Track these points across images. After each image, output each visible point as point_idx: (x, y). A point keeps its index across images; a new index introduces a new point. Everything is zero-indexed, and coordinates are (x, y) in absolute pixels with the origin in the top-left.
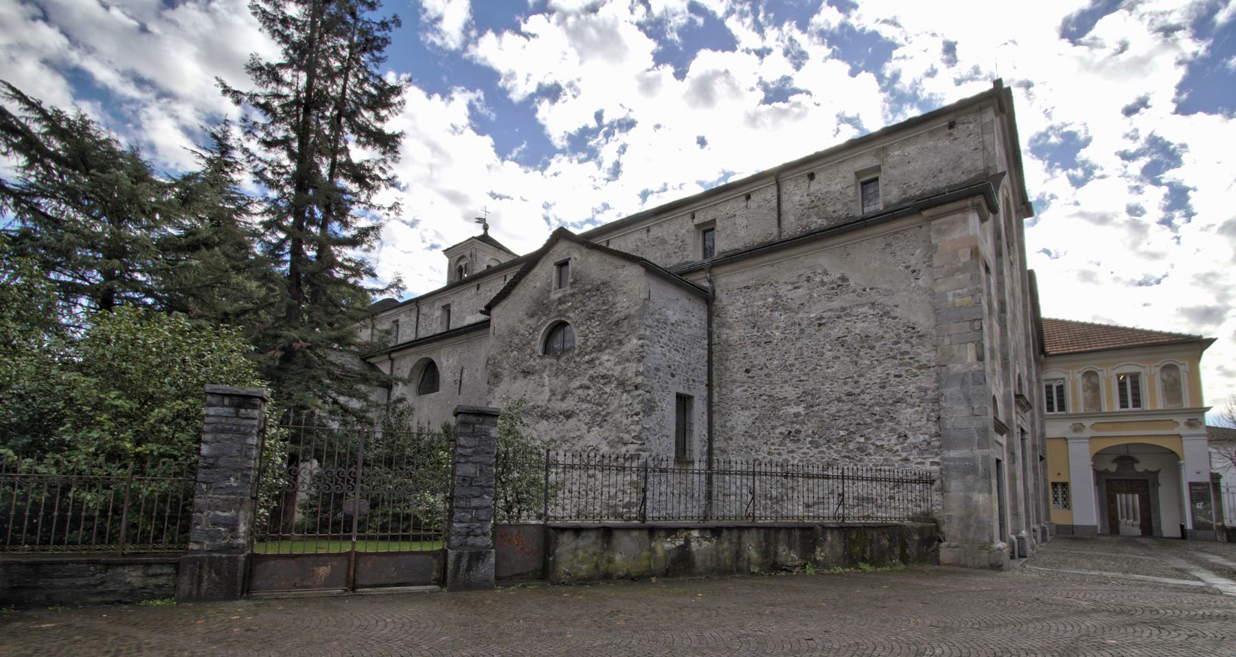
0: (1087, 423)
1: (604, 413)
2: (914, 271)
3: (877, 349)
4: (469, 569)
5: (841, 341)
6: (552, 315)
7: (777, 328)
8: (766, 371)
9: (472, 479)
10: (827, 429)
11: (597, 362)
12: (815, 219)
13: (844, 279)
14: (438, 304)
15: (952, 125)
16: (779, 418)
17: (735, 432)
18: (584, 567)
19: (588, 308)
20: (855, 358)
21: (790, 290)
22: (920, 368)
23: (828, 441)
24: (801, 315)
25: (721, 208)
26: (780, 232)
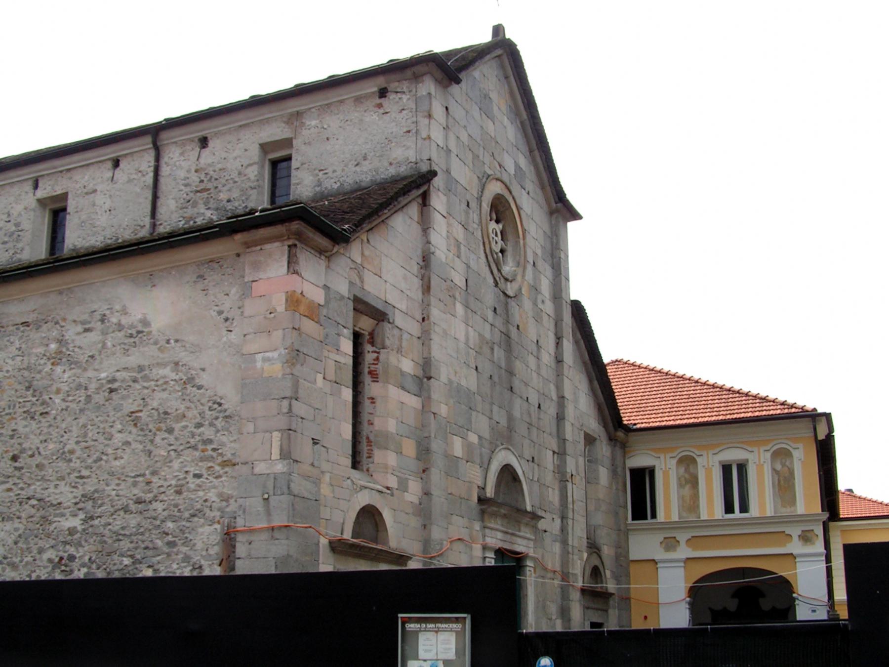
0: (682, 537)
2: (227, 320)
3: (176, 433)
5: (134, 418)
7: (58, 391)
8: (38, 459)
12: (202, 209)
15: (383, 93)
16: (48, 536)
21: (79, 334)
22: (225, 464)
24: (90, 373)
25: (77, 176)
26: (154, 226)
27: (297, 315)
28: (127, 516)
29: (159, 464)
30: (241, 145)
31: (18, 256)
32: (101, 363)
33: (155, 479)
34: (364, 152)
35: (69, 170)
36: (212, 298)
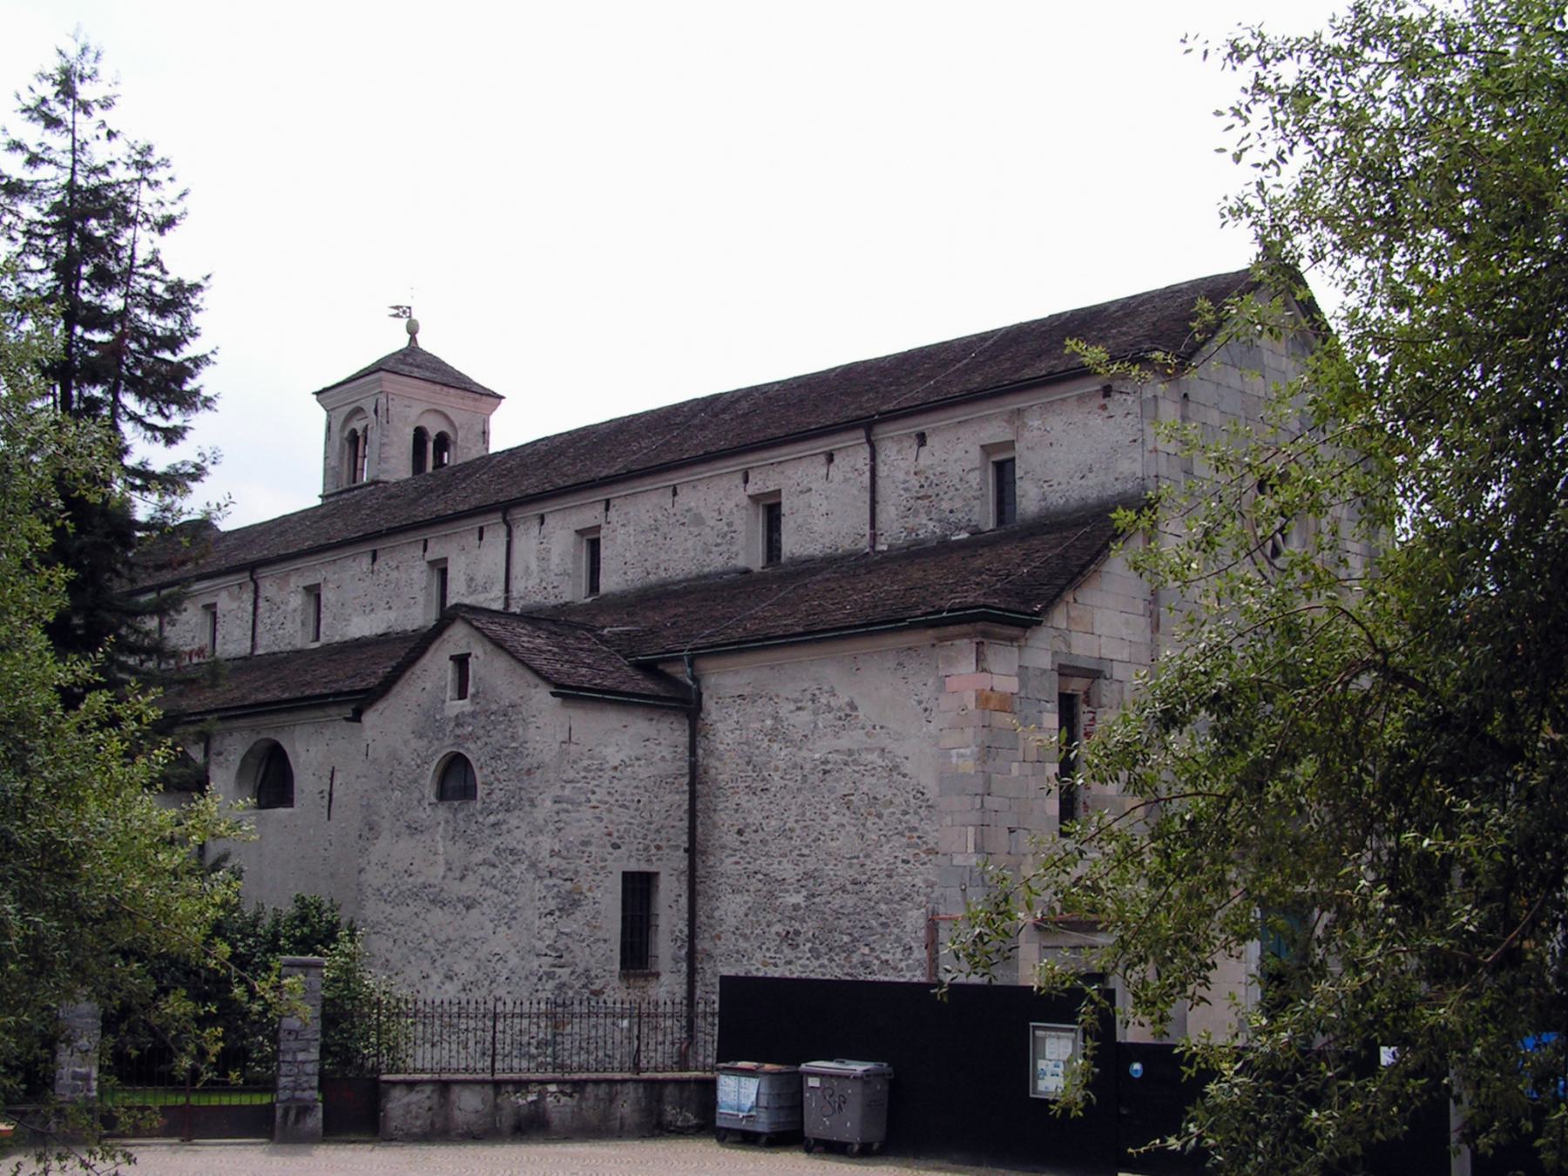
1: (512, 906)
2: (926, 710)
4: (297, 1120)
6: (448, 741)
7: (776, 769)
8: (762, 835)
9: (297, 1033)
10: (830, 932)
11: (504, 827)
13: (853, 707)
14: (297, 582)
17: (724, 927)
18: (418, 1123)
19: (492, 740)
20: (862, 830)
21: (791, 712)
22: (929, 852)
23: (831, 950)
24: (804, 753)
25: (789, 470)
27: (987, 712)
28: (845, 896)
29: (871, 848)
30: (961, 446)
31: (733, 562)
32: (814, 743)
33: (868, 862)
34: (1089, 462)
35: (780, 463)
36: (912, 687)
